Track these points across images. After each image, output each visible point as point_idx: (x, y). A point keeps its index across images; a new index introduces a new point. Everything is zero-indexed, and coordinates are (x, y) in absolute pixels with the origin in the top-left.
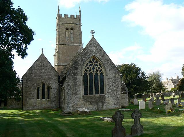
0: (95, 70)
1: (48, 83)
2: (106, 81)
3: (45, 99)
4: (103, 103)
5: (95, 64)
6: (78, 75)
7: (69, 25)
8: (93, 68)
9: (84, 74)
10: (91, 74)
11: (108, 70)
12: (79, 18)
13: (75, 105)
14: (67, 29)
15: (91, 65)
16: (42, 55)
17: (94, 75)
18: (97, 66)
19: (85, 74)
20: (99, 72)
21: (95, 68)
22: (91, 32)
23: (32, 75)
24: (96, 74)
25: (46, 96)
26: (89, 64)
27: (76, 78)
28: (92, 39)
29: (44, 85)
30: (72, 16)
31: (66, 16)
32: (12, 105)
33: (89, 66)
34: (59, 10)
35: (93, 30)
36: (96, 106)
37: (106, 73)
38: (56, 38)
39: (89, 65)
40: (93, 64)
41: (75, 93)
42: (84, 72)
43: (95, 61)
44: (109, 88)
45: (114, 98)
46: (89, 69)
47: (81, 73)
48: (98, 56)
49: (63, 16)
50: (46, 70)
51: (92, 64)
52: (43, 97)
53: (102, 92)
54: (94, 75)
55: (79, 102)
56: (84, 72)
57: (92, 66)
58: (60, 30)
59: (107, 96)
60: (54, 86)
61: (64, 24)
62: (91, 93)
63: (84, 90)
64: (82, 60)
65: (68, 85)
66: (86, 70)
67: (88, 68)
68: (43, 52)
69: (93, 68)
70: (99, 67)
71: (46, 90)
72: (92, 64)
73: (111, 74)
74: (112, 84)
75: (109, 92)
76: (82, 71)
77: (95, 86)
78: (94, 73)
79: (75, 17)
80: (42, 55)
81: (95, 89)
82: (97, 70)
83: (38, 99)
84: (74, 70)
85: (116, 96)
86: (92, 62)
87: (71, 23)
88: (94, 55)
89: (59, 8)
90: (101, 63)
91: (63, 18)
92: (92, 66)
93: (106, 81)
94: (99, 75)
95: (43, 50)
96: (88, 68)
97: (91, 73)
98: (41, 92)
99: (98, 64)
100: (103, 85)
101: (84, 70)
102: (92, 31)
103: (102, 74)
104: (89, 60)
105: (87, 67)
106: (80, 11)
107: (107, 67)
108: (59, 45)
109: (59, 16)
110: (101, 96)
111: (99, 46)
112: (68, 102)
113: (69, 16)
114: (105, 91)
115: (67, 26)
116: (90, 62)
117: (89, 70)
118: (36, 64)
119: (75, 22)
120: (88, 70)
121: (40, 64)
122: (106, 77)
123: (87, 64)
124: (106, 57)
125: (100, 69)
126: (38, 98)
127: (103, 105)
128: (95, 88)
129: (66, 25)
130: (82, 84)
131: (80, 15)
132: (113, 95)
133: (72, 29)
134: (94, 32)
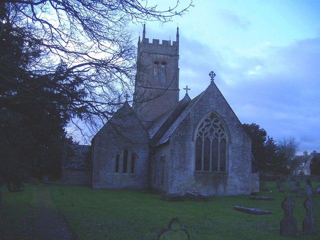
0: (214, 133)
3: (126, 174)
4: (225, 184)
8: (212, 130)
10: (207, 139)
12: (176, 44)
13: (181, 185)
14: (156, 63)
15: (207, 126)
18: (217, 127)
19: (199, 139)
20: (219, 136)
21: (213, 131)
22: (210, 75)
25: (129, 170)
26: (205, 124)
28: (211, 85)
29: (126, 152)
31: (156, 41)
33: (206, 126)
37: (230, 139)
39: (204, 125)
42: (198, 135)
43: (214, 119)
47: (193, 136)
49: (151, 42)
60: (142, 155)
61: (152, 55)
65: (172, 154)
66: (199, 132)
67: (203, 130)
69: (212, 130)
71: (129, 159)
72: (210, 124)
73: (237, 141)
76: (194, 133)
78: (211, 139)
79: (161, 43)
83: (116, 173)
89: (144, 28)
90: (223, 123)
93: (230, 152)
94: (220, 141)
96: (203, 130)
97: (207, 137)
98: (121, 162)
99: (218, 124)
101: (197, 132)
103: (224, 140)
104: (205, 118)
105: (201, 129)
106: (178, 36)
112: (172, 181)
114: (228, 166)
116: (207, 120)
125: (222, 133)
126: (117, 171)
129: (155, 56)
131: (178, 42)
133: (164, 63)
134: (215, 75)
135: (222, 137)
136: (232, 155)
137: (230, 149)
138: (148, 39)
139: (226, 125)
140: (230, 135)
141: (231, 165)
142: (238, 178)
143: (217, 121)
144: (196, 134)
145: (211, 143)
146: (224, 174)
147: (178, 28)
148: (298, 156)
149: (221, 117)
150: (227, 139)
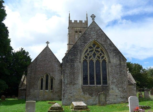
1: (51, 74)
2: (110, 69)
5: (96, 50)
6: (76, 62)
7: (77, 28)
8: (94, 55)
9: (84, 61)
10: (92, 62)
11: (111, 56)
14: (76, 32)
15: (91, 51)
16: (47, 47)
17: (95, 62)
18: (99, 52)
19: (85, 61)
20: (101, 58)
21: (96, 54)
23: (36, 67)
24: (98, 62)
26: (89, 50)
27: (74, 65)
28: (93, 23)
29: (47, 76)
30: (81, 22)
31: (76, 21)
32: (22, 96)
33: (90, 52)
34: (69, 17)
35: (93, 15)
36: (97, 99)
37: (109, 59)
38: (120, 110)
40: (94, 50)
41: (72, 83)
42: (84, 58)
43: (96, 46)
44: (113, 78)
45: (120, 89)
46: (90, 55)
47: (80, 59)
48: (100, 41)
49: (73, 21)
50: (50, 61)
51: (93, 50)
52: (47, 88)
53: (105, 82)
54: (95, 62)
55: (77, 93)
56: (84, 58)
57: (93, 52)
58: (71, 33)
59: (111, 87)
61: (74, 28)
62: (92, 83)
63: (84, 79)
64: (81, 45)
66: (85, 56)
67: (88, 54)
68: (48, 44)
69: (94, 55)
70: (101, 53)
71: (49, 81)
74: (117, 72)
75: (113, 83)
76: (80, 57)
77: (96, 75)
79: (78, 22)
80: (47, 47)
81: (97, 79)
82: (99, 57)
83: (41, 90)
84: (72, 57)
85: (122, 87)
86: (92, 48)
87: (80, 27)
88: (94, 40)
89: (87, 15)
91: (73, 23)
92: (93, 52)
93: (109, 69)
94: (101, 62)
95: (48, 43)
96: (88, 54)
98: (44, 83)
99: (99, 50)
100: (106, 74)
101: (83, 56)
102: (92, 16)
103: (104, 61)
106: (87, 18)
107: (110, 53)
108: (70, 45)
109: (70, 22)
110: (103, 86)
111: (100, 30)
112: (64, 93)
113: (83, 22)
115: (76, 29)
116: (90, 47)
117: (90, 57)
118: (40, 56)
119: (83, 26)
120: (88, 57)
121: (44, 56)
122: (110, 65)
123: (87, 50)
124: (109, 42)
125: (102, 55)
126: (42, 89)
127: (106, 98)
128: (97, 77)
129: (75, 28)
130: (80, 72)
131: (87, 21)
132: (118, 86)
133: (80, 32)
134: (95, 17)
135: (103, 59)
136: (111, 72)
137: (109, 67)
138: (71, 21)
139: (105, 49)
140: (108, 57)
141: (111, 78)
142: (118, 89)
143: (98, 48)
144: (82, 58)
145: (95, 63)
146: (106, 87)
147: (87, 14)
148: (23, 103)
149: (101, 44)
150: (107, 61)
